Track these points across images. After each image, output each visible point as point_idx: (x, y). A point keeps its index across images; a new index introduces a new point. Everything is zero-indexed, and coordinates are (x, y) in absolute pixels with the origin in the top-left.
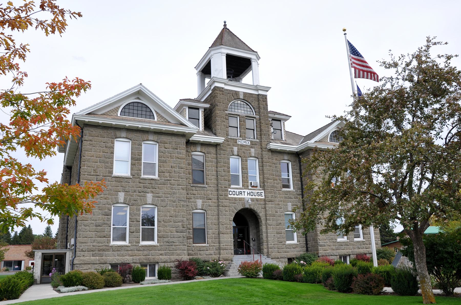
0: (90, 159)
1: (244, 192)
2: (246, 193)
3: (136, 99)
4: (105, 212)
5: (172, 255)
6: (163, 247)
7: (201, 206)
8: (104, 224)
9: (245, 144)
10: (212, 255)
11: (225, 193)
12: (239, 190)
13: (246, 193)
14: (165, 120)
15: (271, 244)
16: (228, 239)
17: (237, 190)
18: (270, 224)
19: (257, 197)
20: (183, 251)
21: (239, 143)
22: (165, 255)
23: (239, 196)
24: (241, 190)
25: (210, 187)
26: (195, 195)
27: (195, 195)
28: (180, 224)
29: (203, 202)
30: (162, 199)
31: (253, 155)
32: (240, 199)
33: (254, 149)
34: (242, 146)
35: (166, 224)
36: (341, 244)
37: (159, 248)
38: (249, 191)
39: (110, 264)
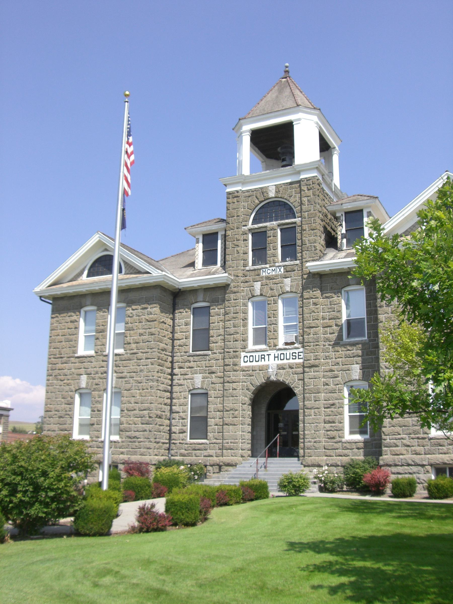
0: (56, 338)
1: (269, 355)
2: (272, 357)
3: (103, 251)
4: (68, 401)
5: (134, 455)
6: (124, 444)
7: (200, 383)
8: (66, 414)
9: (274, 273)
10: (212, 456)
11: (233, 362)
12: (260, 354)
13: (272, 357)
14: (135, 271)
15: (310, 442)
16: (241, 430)
17: (257, 354)
18: (309, 406)
19: (291, 361)
20: (148, 450)
21: (264, 274)
22: (127, 454)
23: (260, 363)
24: (263, 353)
25: (215, 353)
26: (192, 368)
27: (192, 368)
28: (146, 412)
29: (204, 378)
30: (126, 379)
31: (288, 289)
32: (261, 369)
33: (289, 279)
34: (268, 278)
35: (130, 413)
36: (437, 443)
37: (121, 444)
38: (277, 353)
39: (431, 465)
